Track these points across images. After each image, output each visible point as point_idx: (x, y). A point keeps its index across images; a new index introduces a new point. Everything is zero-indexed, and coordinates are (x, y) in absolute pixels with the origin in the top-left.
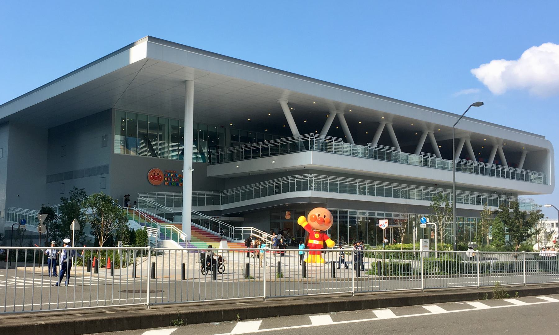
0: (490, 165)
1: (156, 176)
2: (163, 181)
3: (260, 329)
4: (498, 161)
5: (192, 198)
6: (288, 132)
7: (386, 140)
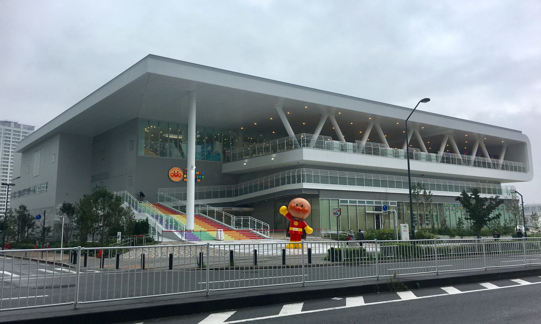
0: (473, 157)
1: (176, 174)
2: (182, 177)
3: (302, 311)
4: (480, 153)
5: (195, 192)
6: (285, 133)
7: (375, 138)
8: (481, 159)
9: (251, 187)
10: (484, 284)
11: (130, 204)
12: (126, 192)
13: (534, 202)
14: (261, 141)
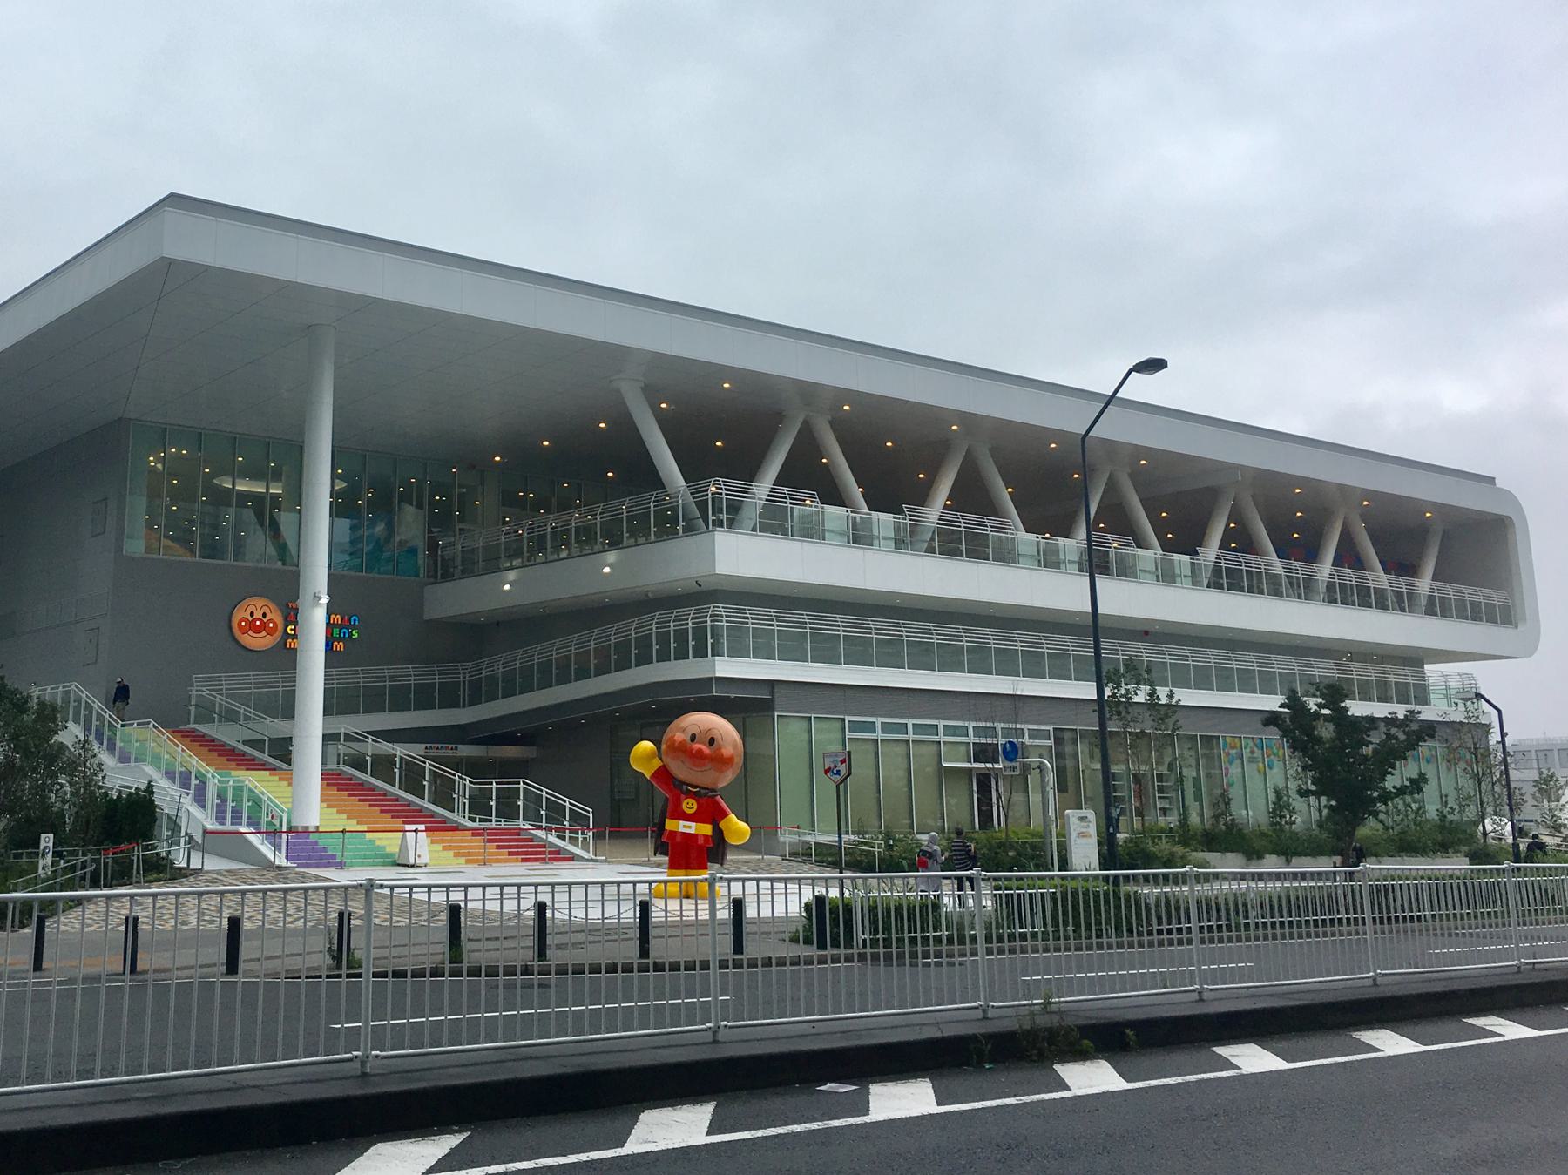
0: (1325, 570)
1: (258, 623)
4: (1348, 556)
8: (1351, 576)
9: (527, 672)
10: (1367, 1037)
11: (87, 729)
12: (74, 686)
13: (1545, 733)
14: (565, 506)
